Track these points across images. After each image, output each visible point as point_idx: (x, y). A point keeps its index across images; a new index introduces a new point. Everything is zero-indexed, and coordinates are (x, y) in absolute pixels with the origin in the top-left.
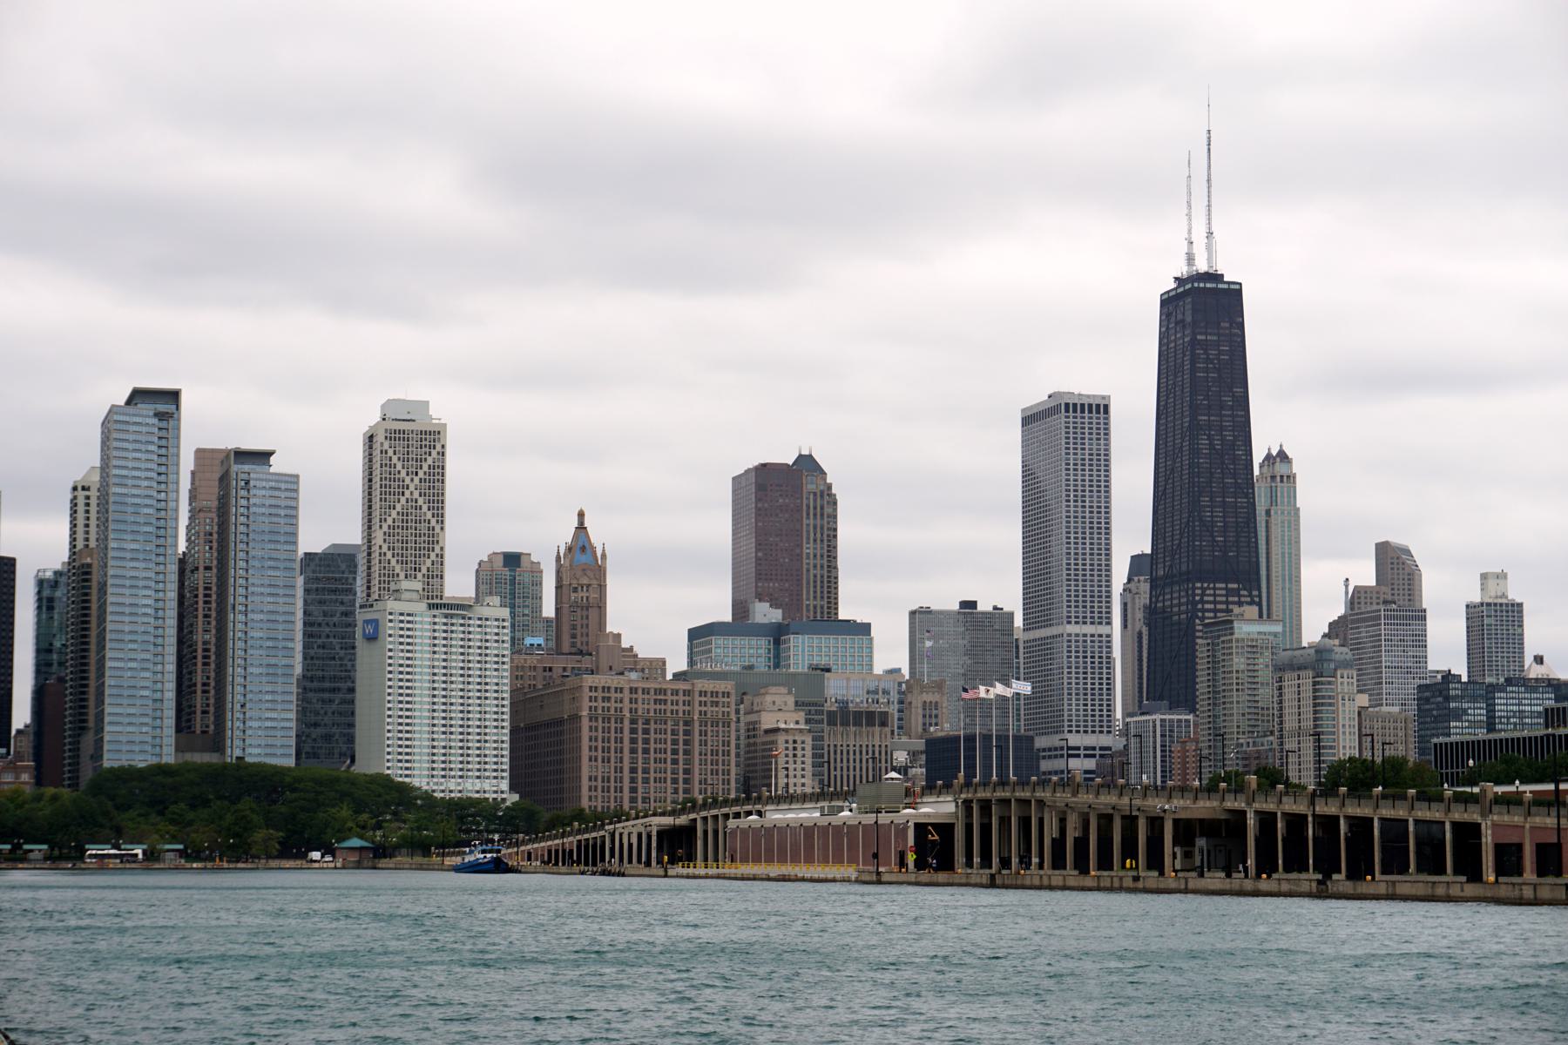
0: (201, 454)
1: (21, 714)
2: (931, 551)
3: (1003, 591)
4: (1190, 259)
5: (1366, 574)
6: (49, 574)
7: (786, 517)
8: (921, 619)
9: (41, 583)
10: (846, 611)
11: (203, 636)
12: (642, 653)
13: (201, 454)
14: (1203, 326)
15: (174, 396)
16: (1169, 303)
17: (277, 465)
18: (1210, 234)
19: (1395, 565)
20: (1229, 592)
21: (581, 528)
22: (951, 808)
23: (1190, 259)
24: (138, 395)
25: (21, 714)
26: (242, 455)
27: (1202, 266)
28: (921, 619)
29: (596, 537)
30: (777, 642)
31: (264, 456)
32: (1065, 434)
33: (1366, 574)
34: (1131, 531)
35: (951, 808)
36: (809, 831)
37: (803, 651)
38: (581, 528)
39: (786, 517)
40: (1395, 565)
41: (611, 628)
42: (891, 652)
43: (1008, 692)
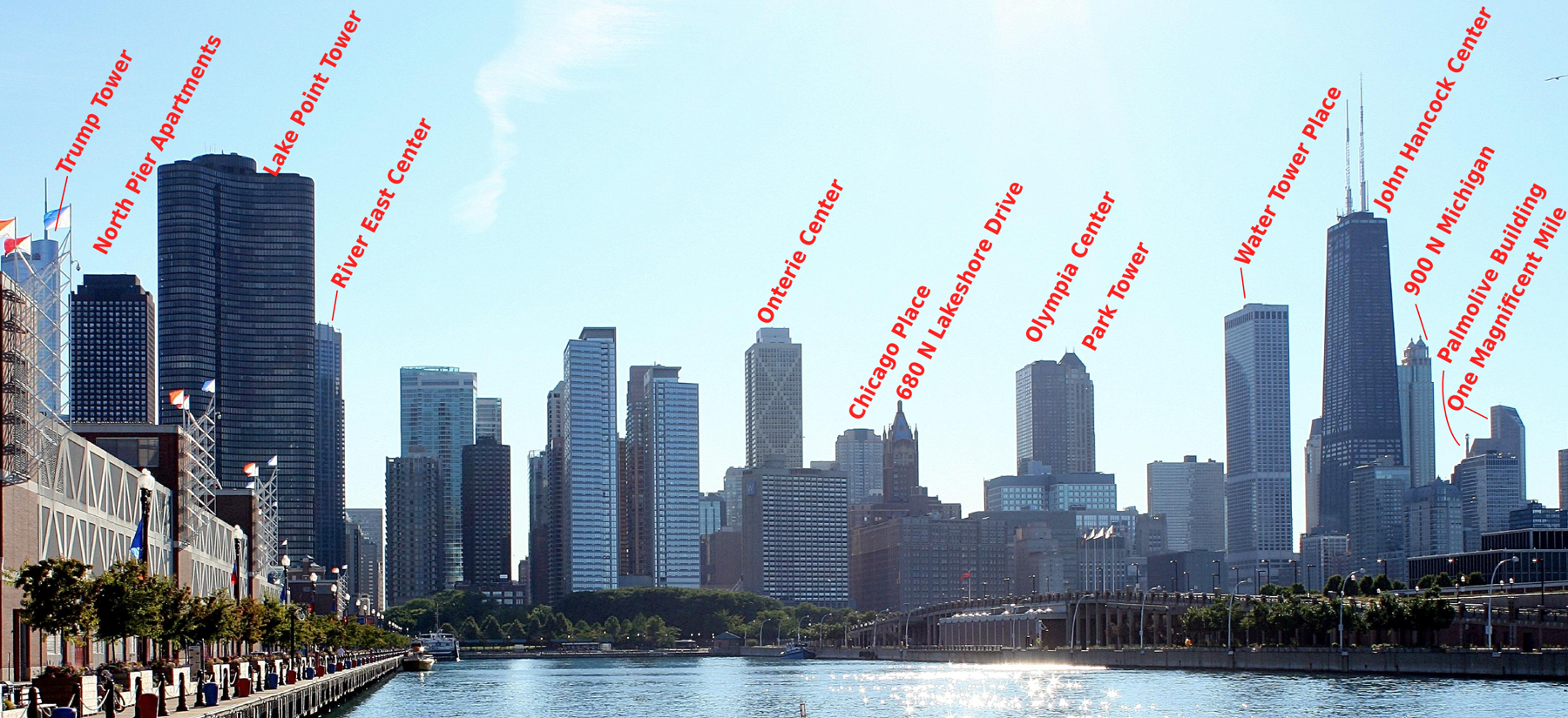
0: (637, 372)
1: (520, 549)
2: (1158, 422)
3: (1213, 447)
4: (1349, 202)
5: (1484, 431)
6: (537, 454)
7: (1058, 404)
8: (1157, 472)
9: (532, 461)
10: (1101, 466)
11: (638, 497)
12: (944, 500)
13: (637, 372)
14: (1359, 248)
15: (611, 332)
16: (1333, 234)
17: (683, 377)
18: (1363, 184)
19: (1507, 422)
20: (1379, 446)
21: (900, 414)
22: (1064, 609)
23: (1349, 202)
24: (588, 332)
25: (520, 549)
26: (659, 371)
27: (1357, 208)
28: (1157, 472)
29: (911, 421)
30: (1048, 489)
31: (674, 371)
32: (1259, 332)
33: (1484, 431)
34: (1306, 400)
35: (1064, 609)
36: (983, 623)
37: (1066, 495)
38: (900, 414)
39: (1058, 404)
40: (1507, 422)
41: (922, 483)
42: (1133, 495)
43: (78, 515)
